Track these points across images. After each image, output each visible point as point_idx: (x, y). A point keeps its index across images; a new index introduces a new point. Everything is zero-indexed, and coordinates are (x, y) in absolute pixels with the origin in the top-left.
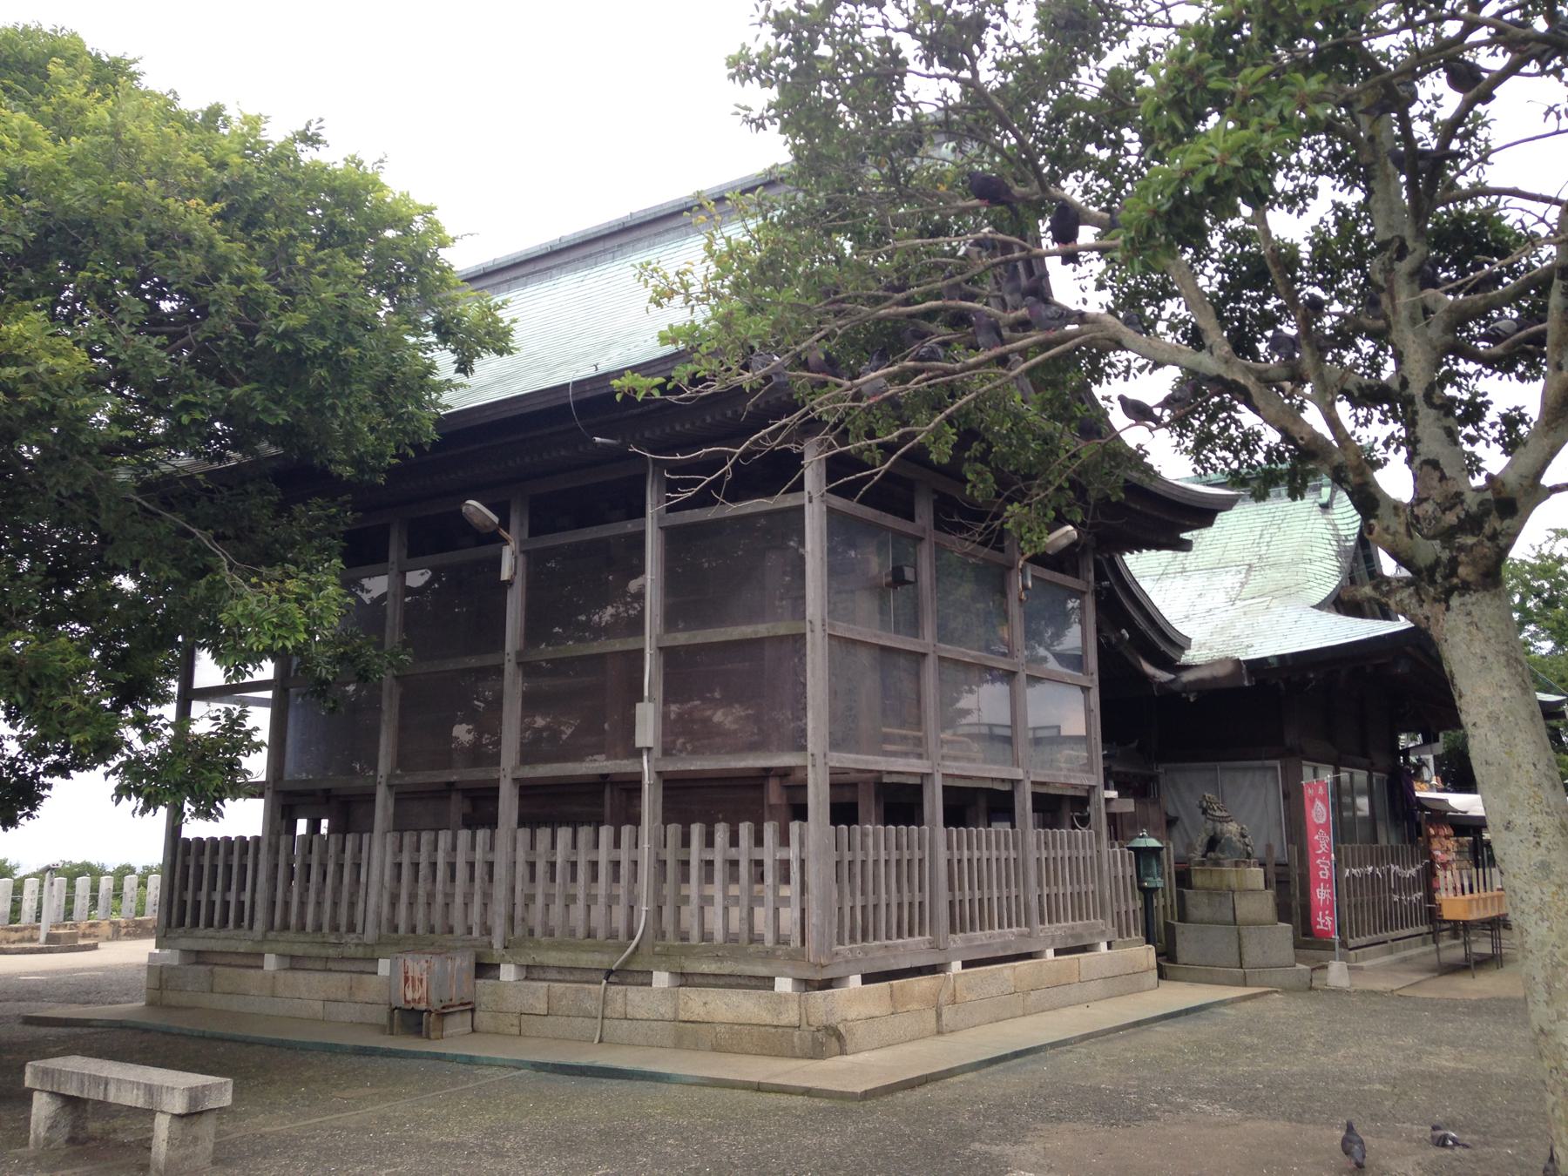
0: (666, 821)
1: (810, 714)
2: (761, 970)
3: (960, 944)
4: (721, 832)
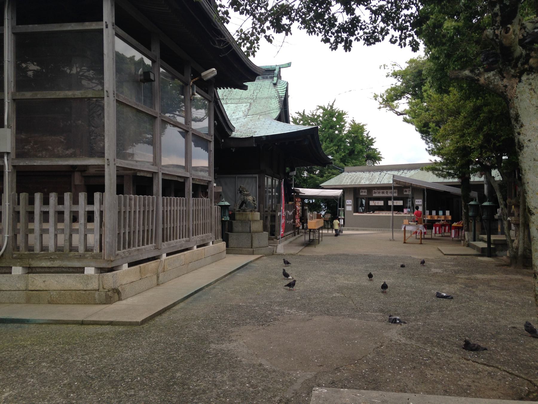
0: (19, 192)
1: (106, 140)
2: (77, 264)
3: (166, 246)
4: (53, 198)
